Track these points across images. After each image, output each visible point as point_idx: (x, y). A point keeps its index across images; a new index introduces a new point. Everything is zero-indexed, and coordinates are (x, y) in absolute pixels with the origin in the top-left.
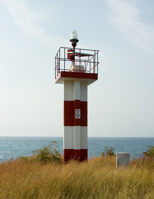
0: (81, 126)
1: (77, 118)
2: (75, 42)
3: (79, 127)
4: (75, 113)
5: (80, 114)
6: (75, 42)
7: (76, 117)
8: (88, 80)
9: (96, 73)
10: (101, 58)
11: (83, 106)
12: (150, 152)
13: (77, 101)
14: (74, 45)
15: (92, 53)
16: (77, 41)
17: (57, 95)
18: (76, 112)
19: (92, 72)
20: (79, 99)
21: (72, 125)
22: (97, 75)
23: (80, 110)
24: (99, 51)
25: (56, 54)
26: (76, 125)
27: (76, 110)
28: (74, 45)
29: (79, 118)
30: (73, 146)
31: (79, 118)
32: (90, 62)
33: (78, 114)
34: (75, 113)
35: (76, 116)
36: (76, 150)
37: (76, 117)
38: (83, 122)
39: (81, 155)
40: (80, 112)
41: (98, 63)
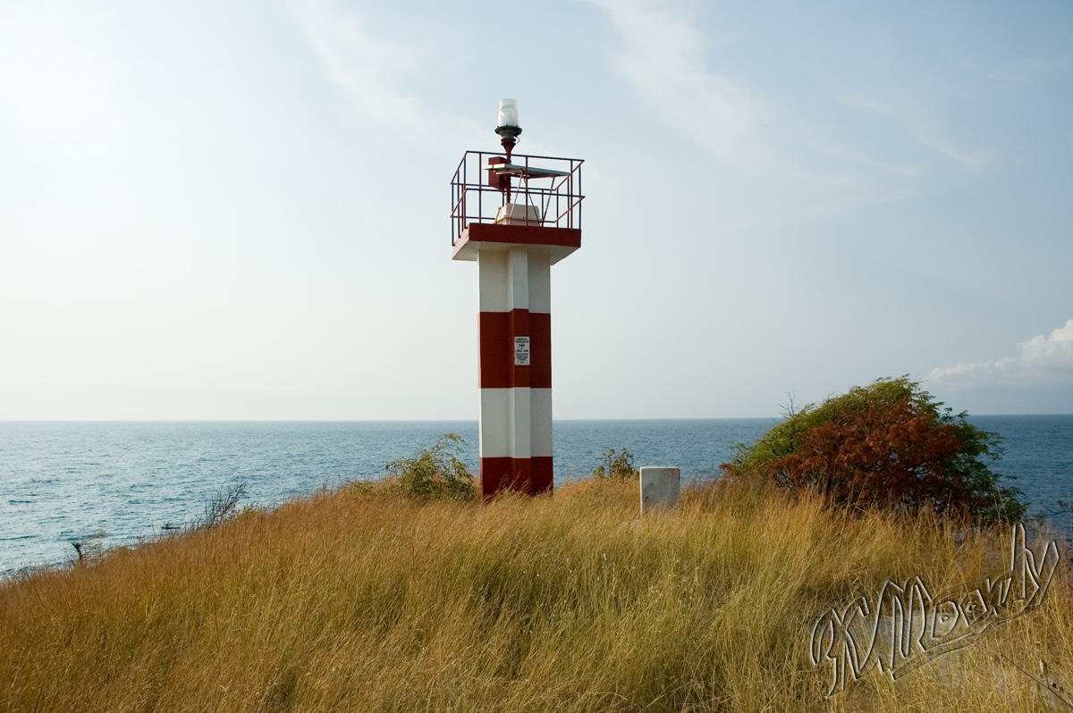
2: (510, 134)
4: (514, 349)
6: (510, 134)
7: (517, 362)
8: (553, 248)
9: (576, 226)
11: (537, 326)
14: (509, 144)
15: (564, 167)
16: (517, 131)
18: (516, 346)
22: (579, 231)
23: (528, 338)
24: (583, 161)
27: (516, 338)
28: (509, 144)
29: (527, 362)
30: (508, 448)
31: (527, 362)
32: (558, 195)
33: (522, 350)
34: (514, 349)
36: (516, 459)
37: (517, 362)
38: (539, 375)
40: (527, 346)
41: (582, 197)
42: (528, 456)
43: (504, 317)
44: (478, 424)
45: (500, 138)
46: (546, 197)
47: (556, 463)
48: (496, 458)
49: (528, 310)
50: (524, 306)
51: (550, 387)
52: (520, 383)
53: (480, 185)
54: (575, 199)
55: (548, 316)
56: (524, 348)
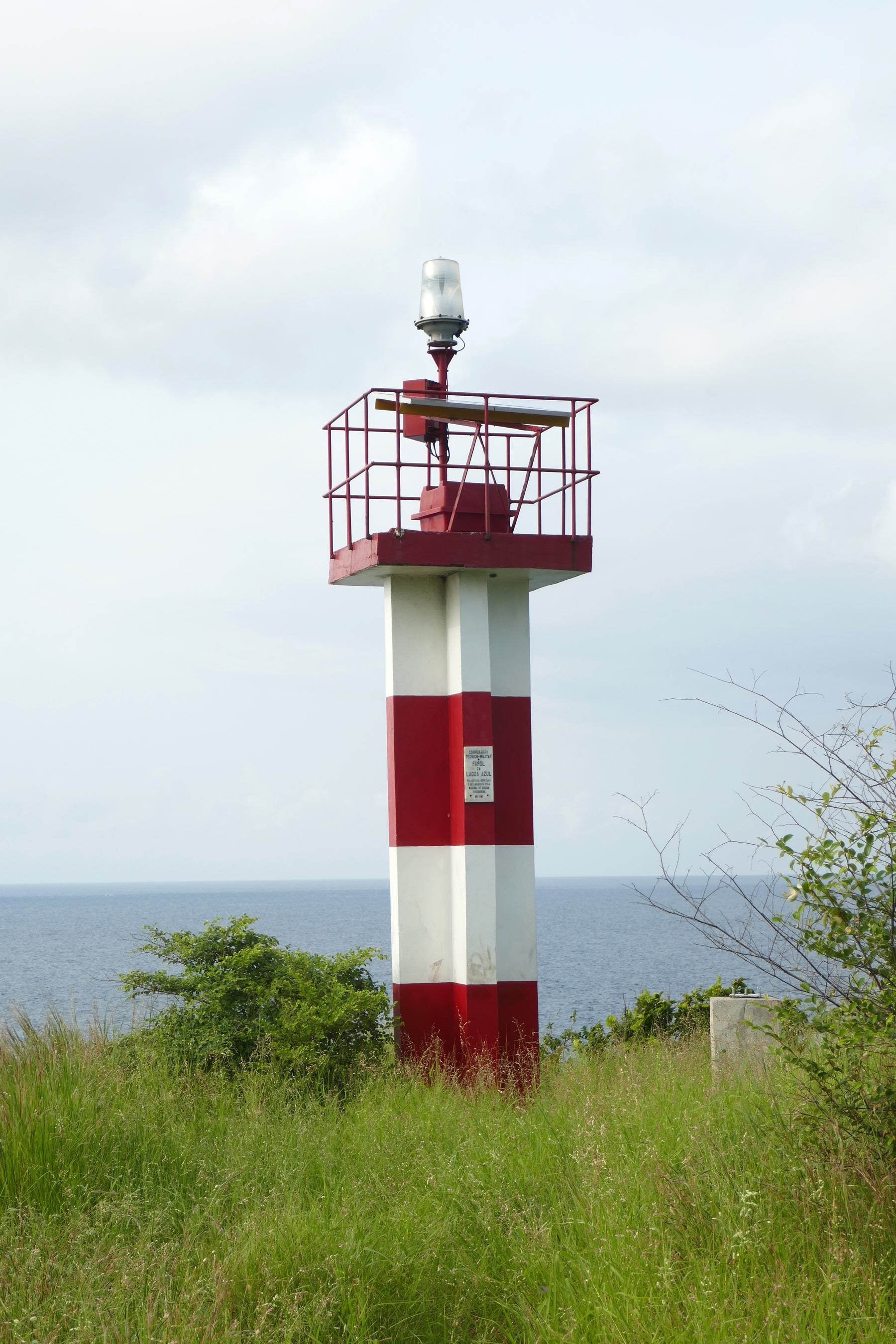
0: (496, 844)
1: (474, 800)
2: (445, 333)
3: (488, 852)
4: (458, 770)
5: (492, 778)
6: (445, 333)
7: (469, 796)
8: (532, 572)
9: (582, 531)
10: (607, 438)
11: (504, 722)
12: (784, 1127)
13: (472, 701)
14: (443, 355)
15: (565, 407)
16: (460, 325)
17: (371, 655)
18: (468, 765)
19: (552, 528)
20: (487, 689)
21: (442, 836)
22: (587, 541)
23: (490, 750)
24: (594, 401)
25: (361, 395)
26: (470, 840)
27: (467, 749)
28: (443, 355)
29: (489, 796)
30: (451, 970)
31: (489, 796)
32: (348, 429)
33: (477, 773)
34: (458, 770)
35: (466, 783)
36: (476, 992)
37: (469, 796)
38: (508, 820)
39: (479, 1027)
40: (488, 764)
41: (591, 473)
42: (492, 980)
43: (439, 706)
44: (386, 893)
45: (424, 338)
46: (535, 465)
47: (540, 988)
48: (398, 876)
49: (489, 693)
50: (482, 685)
51: (532, 843)
52: (474, 837)
53: (540, 470)
54: (578, 475)
55: (529, 698)
56: (483, 769)
